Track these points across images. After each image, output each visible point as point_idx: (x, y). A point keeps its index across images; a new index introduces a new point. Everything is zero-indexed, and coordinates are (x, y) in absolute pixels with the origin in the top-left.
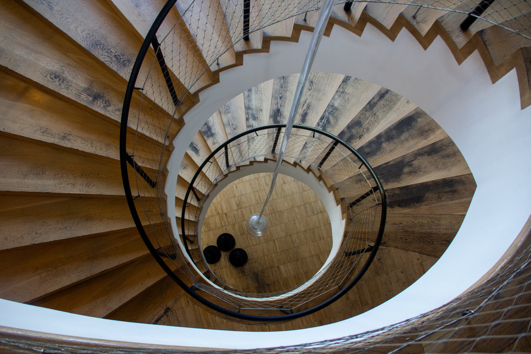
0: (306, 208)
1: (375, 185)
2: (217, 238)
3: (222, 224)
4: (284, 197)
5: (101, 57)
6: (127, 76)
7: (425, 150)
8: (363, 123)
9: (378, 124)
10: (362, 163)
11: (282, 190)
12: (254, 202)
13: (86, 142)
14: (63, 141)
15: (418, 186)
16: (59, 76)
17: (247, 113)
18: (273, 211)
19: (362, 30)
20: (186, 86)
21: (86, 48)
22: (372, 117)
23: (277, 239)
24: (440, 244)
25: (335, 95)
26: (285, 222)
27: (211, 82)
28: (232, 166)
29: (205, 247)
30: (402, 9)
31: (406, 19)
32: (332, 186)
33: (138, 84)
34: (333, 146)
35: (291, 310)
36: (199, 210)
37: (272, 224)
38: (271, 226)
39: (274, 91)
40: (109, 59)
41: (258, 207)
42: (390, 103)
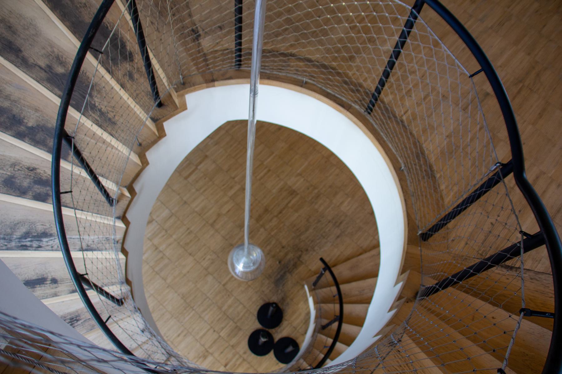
8: (5, 176)
23: (220, 283)
29: (282, 365)
38: (208, 300)
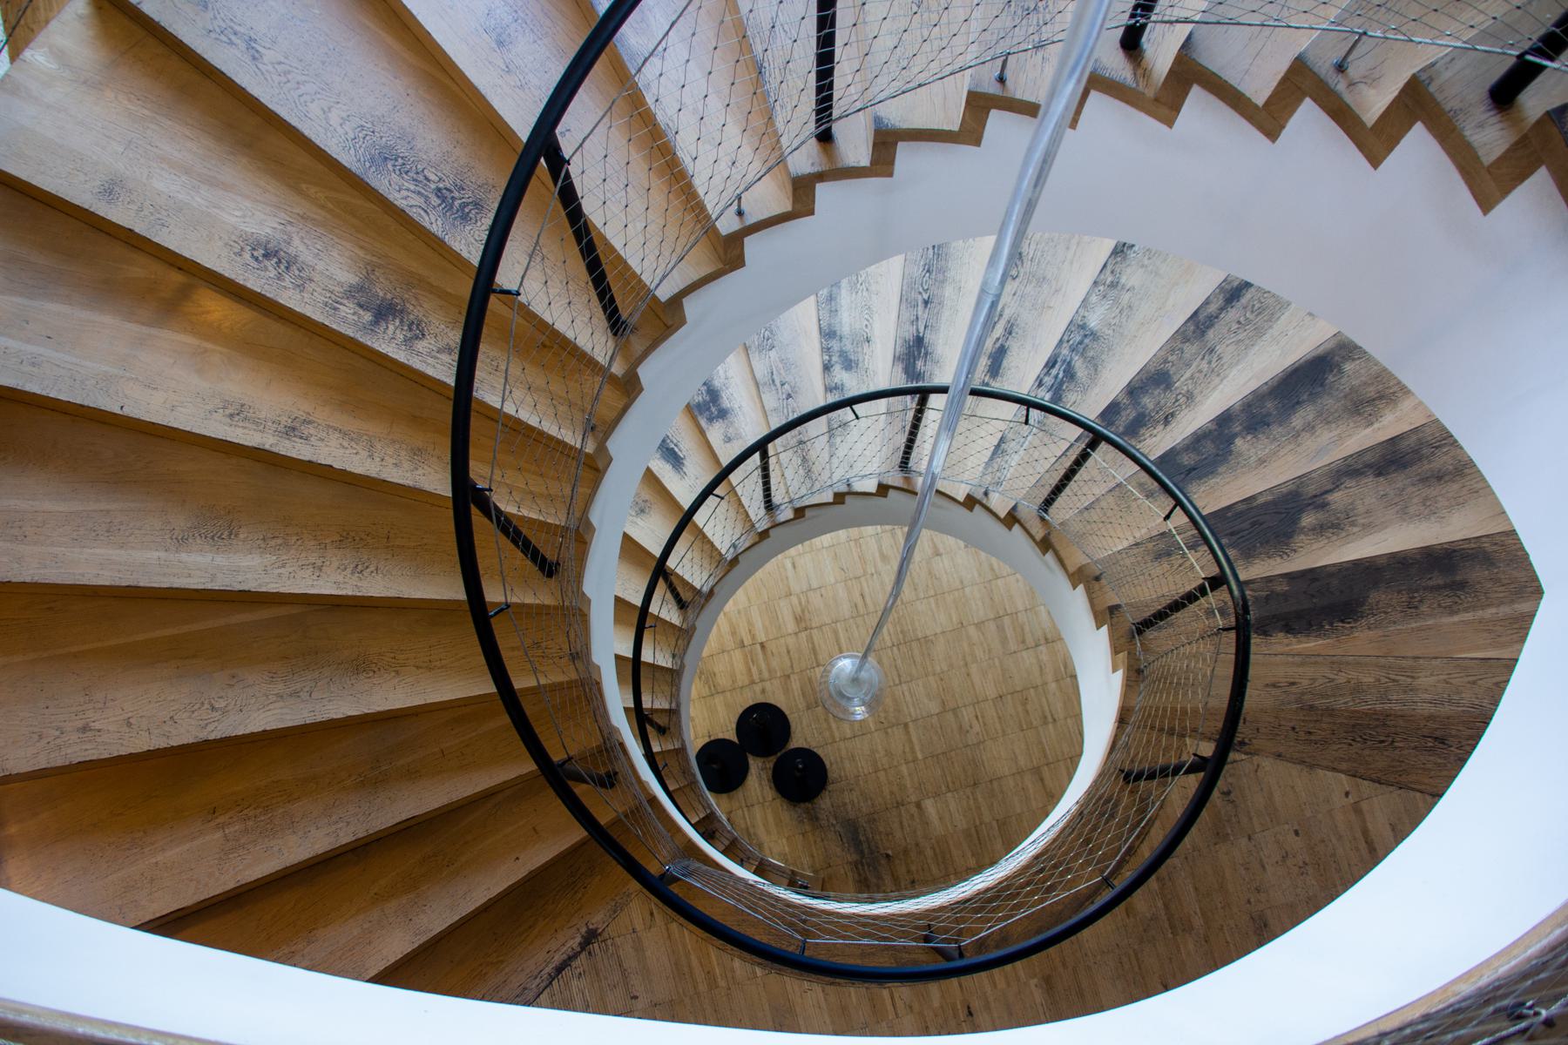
0: (1001, 629)
1: (1214, 571)
2: (737, 716)
3: (751, 676)
4: (936, 595)
5: (397, 195)
6: (474, 252)
7: (1368, 458)
9: (1222, 380)
10: (1174, 503)
11: (930, 573)
12: (846, 610)
13: (353, 444)
14: (287, 442)
15: (1347, 569)
16: (277, 252)
17: (826, 350)
18: (904, 637)
19: (1176, 108)
20: (647, 279)
21: (354, 169)
22: (1203, 359)
24: (1415, 748)
25: (1088, 294)
26: (938, 669)
27: (721, 266)
28: (783, 507)
29: (700, 743)
30: (1301, 43)
31: (1314, 73)
32: (1080, 570)
33: (506, 277)
34: (1084, 450)
35: (960, 947)
36: (683, 636)
37: (899, 676)
38: (897, 682)
39: (905, 281)
40: (419, 201)
41: (857, 627)
42: (1257, 315)
